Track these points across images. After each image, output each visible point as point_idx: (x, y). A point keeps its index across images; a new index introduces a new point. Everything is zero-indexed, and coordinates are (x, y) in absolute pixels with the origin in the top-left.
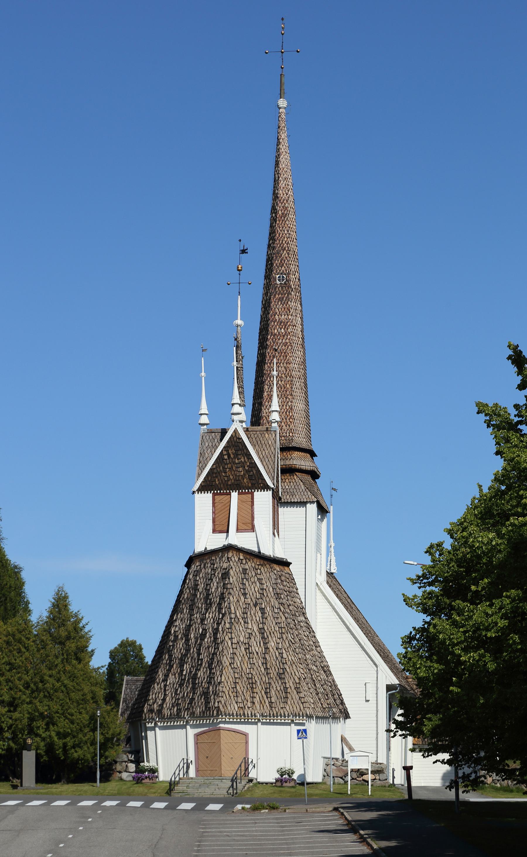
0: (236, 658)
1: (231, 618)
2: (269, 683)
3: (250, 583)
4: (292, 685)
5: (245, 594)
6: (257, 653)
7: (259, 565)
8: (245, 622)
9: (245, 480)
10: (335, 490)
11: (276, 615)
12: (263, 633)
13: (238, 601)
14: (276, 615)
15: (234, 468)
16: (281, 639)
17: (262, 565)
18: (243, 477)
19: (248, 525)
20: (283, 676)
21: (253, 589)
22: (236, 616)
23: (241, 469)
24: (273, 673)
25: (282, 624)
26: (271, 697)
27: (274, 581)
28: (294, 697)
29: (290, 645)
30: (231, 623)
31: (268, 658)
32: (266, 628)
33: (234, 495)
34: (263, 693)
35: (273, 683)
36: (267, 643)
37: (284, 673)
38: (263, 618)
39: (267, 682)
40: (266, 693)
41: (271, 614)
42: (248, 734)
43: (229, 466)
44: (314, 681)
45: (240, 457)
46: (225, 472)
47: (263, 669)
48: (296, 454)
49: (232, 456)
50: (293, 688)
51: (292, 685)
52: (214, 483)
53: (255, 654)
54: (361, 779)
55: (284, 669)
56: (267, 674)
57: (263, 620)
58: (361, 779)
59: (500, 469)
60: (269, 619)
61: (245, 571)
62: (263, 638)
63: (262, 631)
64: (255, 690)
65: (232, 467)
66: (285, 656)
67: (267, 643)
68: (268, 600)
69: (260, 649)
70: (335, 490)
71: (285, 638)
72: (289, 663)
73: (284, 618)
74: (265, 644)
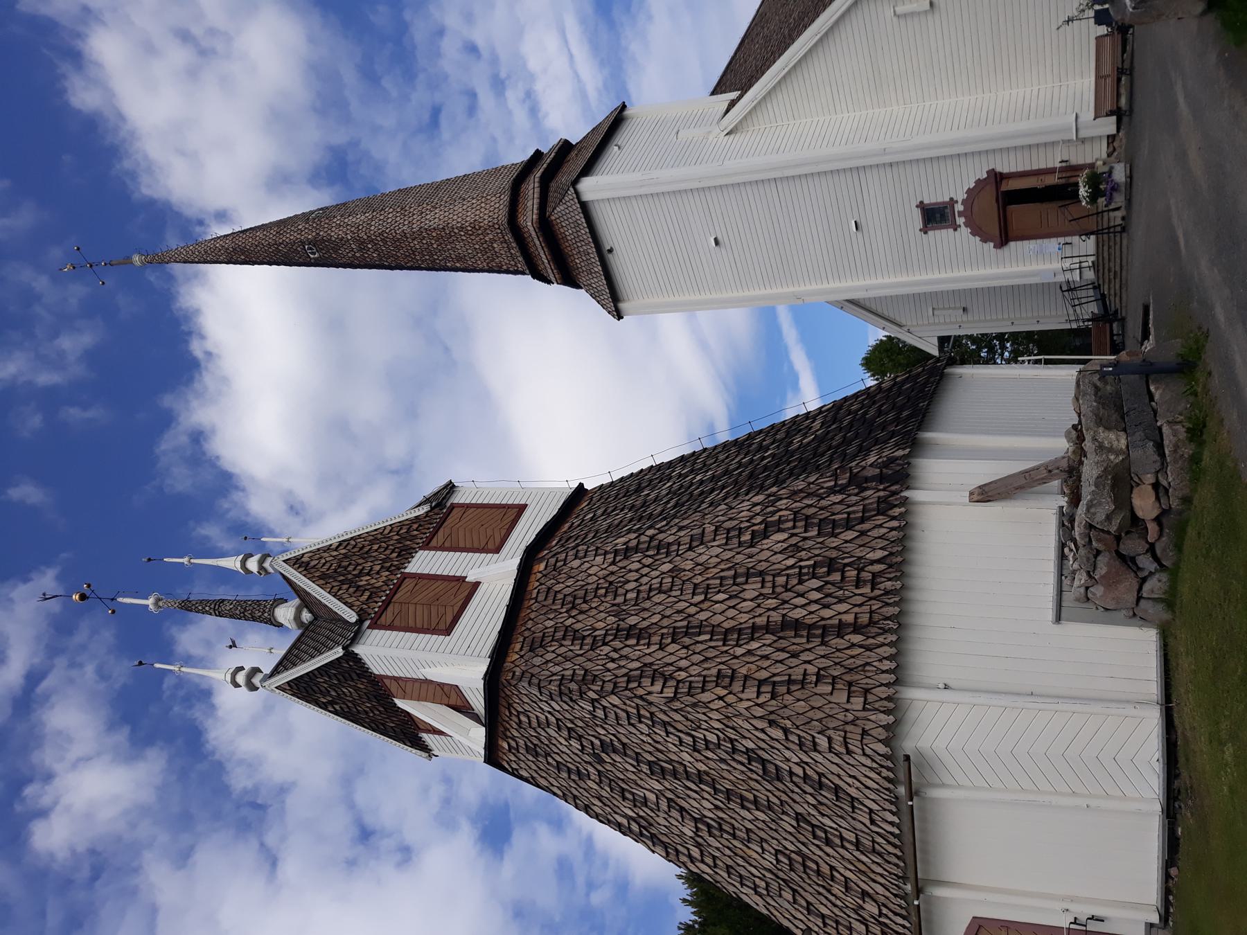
24: (763, 791)
26: (842, 838)
37: (763, 762)
54: (1152, 528)
58: (1152, 528)
61: (533, 750)
63: (657, 770)
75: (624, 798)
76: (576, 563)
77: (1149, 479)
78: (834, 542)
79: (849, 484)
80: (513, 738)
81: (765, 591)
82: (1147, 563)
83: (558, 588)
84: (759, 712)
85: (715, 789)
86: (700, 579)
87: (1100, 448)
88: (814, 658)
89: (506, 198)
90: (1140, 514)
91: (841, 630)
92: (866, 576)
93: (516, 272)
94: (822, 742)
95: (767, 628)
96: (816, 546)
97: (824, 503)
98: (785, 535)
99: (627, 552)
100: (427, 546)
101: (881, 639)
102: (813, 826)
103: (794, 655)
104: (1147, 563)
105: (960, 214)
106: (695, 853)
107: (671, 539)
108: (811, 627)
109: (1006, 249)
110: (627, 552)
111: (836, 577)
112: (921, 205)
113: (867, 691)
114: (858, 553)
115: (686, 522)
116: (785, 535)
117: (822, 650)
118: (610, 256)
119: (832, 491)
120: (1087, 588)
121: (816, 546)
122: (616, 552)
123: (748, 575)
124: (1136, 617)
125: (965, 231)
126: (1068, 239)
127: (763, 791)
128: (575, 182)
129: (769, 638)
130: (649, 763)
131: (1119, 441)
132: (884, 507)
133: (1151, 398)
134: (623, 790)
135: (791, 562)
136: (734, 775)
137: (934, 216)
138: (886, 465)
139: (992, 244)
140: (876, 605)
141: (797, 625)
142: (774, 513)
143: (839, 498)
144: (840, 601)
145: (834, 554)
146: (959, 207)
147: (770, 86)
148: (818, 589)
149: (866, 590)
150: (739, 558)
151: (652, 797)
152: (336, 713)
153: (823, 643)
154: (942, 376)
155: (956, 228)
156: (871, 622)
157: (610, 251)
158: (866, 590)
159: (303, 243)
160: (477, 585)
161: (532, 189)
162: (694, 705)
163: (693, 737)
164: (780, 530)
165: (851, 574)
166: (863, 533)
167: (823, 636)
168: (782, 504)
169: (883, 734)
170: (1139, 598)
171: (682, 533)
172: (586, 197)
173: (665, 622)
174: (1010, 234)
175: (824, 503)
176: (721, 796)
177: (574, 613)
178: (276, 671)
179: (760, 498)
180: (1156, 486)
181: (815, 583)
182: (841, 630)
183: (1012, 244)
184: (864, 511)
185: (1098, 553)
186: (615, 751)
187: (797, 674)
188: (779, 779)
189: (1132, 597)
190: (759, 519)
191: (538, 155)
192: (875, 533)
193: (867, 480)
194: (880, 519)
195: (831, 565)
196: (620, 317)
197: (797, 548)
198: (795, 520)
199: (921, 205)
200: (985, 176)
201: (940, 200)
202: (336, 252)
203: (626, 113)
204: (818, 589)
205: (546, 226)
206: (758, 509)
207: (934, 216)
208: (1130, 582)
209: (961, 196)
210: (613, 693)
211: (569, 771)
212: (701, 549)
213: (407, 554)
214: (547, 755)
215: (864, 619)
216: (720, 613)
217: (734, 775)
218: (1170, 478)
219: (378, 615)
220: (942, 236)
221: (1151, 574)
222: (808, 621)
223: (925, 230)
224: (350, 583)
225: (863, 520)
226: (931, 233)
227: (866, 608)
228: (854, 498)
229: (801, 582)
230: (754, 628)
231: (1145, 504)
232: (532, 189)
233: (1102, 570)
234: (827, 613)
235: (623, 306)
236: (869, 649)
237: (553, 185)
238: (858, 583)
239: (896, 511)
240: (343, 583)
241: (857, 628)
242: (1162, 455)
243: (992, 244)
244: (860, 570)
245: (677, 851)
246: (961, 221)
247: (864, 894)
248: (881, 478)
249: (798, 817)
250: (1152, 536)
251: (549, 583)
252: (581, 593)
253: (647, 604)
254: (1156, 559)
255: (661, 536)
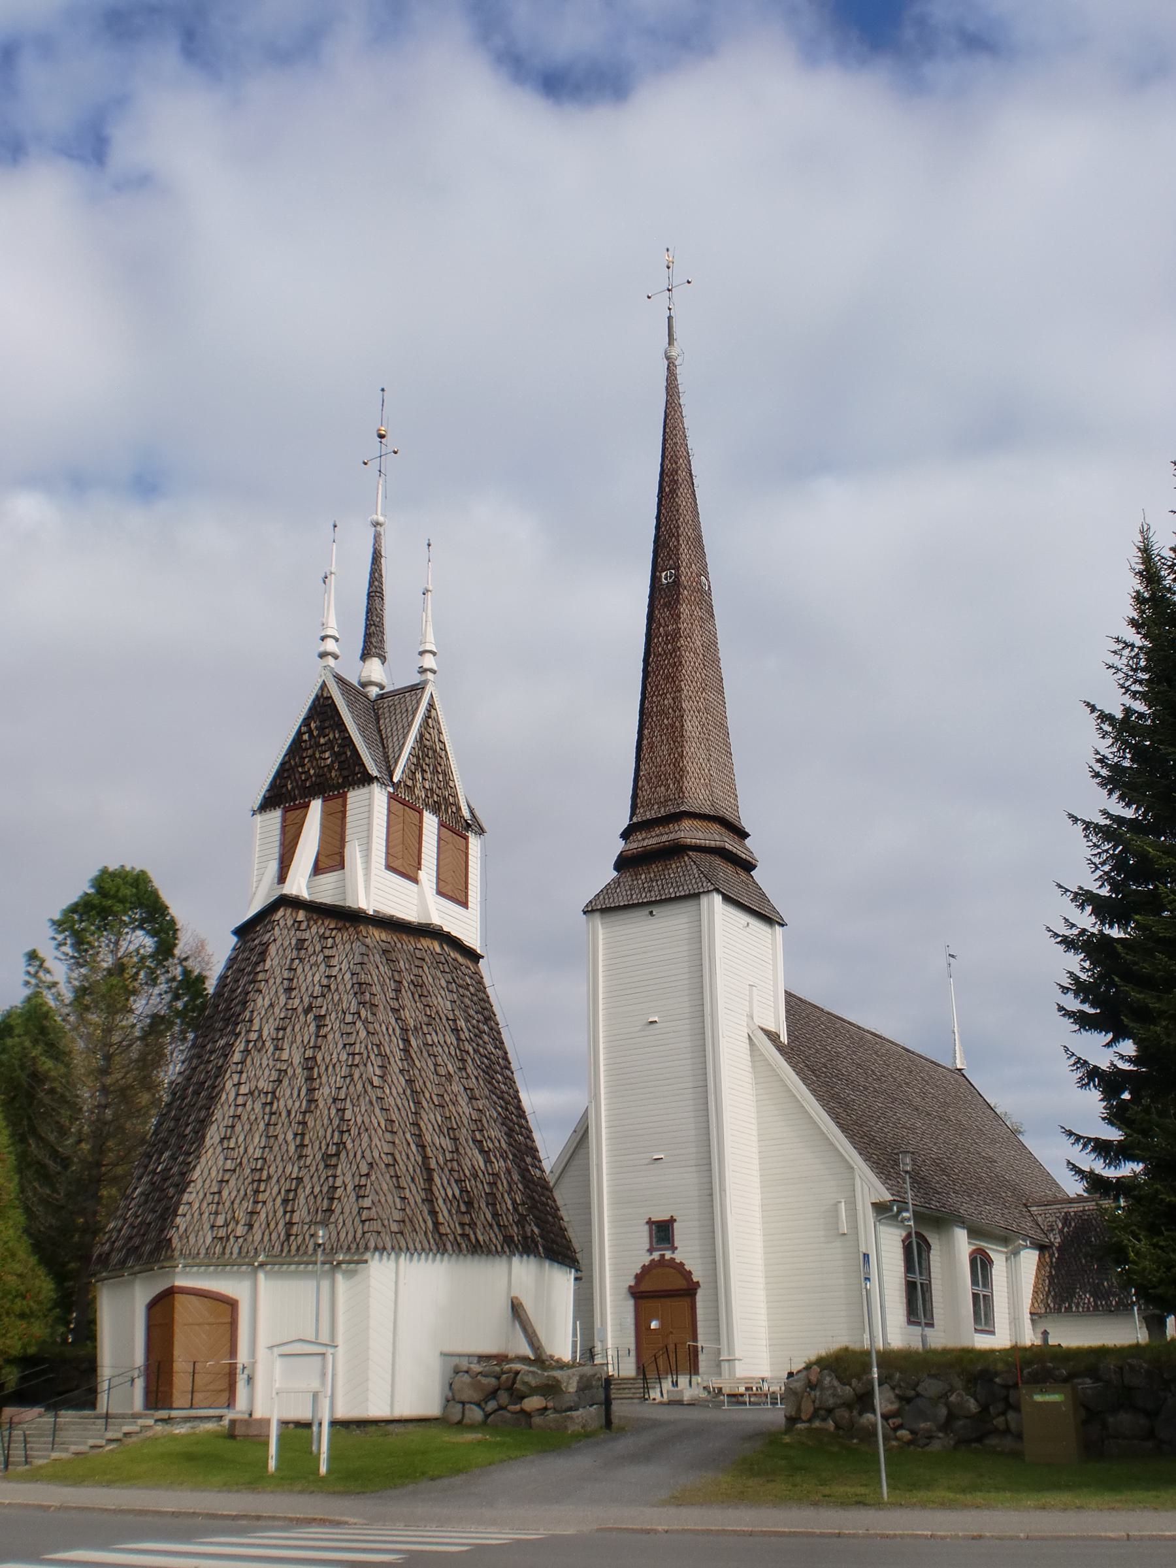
0: (238, 1128)
1: (248, 1042)
2: (297, 1178)
3: (307, 968)
4: (348, 1179)
5: (289, 990)
6: (289, 1112)
7: (332, 929)
8: (277, 1048)
9: (333, 774)
10: (953, 956)
11: (348, 1029)
12: (312, 1069)
13: (272, 1005)
14: (348, 1029)
15: (317, 756)
16: (348, 1080)
17: (339, 930)
18: (330, 767)
19: (331, 859)
20: (333, 1161)
21: (311, 978)
22: (260, 1036)
23: (327, 755)
24: (313, 1153)
25: (357, 1046)
26: (293, 1212)
27: (358, 959)
28: (347, 1210)
29: (366, 1091)
30: (247, 1051)
31: (311, 1124)
32: (319, 1058)
33: (316, 806)
34: (279, 1200)
35: (306, 1180)
36: (315, 1089)
37: (337, 1154)
38: (317, 1036)
39: (294, 1176)
40: (285, 1201)
41: (336, 1027)
42: (237, 1301)
43: (310, 752)
44: (430, 1171)
45: (327, 731)
46: (303, 766)
47: (292, 1148)
48: (686, 823)
49: (315, 733)
50: (350, 1187)
51: (348, 1179)
52: (284, 790)
53: (284, 1114)
54: (518, 1407)
55: (341, 1145)
56: (300, 1157)
57: (316, 1040)
58: (518, 1407)
59: (1089, 853)
60: (330, 1037)
61: (300, 944)
62: (310, 1079)
63: (309, 1064)
64: (261, 1197)
65: (314, 754)
66: (348, 1115)
67: (315, 1089)
68: (336, 998)
69: (297, 1104)
70: (953, 956)
71: (356, 1077)
72: (354, 1131)
73: (363, 1034)
74: (311, 1090)
75: (278, 1029)
76: (444, 984)
77: (550, 1404)
78: (483, 1205)
79: (519, 1214)
80: (309, 927)
81: (447, 1154)
82: (491, 1405)
83: (426, 968)
84: (376, 1154)
85: (305, 1112)
86: (447, 1099)
87: (569, 1378)
88: (415, 1194)
89: (707, 810)
90: (526, 1400)
91: (433, 1213)
92: (468, 1230)
93: (634, 807)
94: (367, 1203)
95: (425, 1158)
96: (479, 1189)
97: (506, 1195)
98: (483, 1168)
99: (456, 1031)
100: (442, 824)
101: (432, 1241)
102: (296, 1190)
103: (413, 1179)
104: (491, 1405)
105: (663, 1255)
106: (244, 1089)
107: (469, 1071)
108: (431, 1190)
109: (629, 1296)
110: (456, 1031)
111: (463, 1209)
112: (672, 1220)
113: (402, 1233)
114: (479, 1223)
115: (481, 1082)
116: (483, 1168)
117: (419, 1200)
118: (647, 912)
119: (514, 1201)
120: (467, 1372)
121: (479, 1189)
122: (454, 1020)
123: (455, 1139)
124: (448, 1401)
125: (646, 1259)
126: (633, 1353)
127: (313, 1153)
128: (718, 890)
129: (419, 1159)
130: (314, 1058)
131: (572, 1388)
132: (508, 1240)
133: (591, 1406)
134: (284, 1029)
135: (468, 1174)
136: (320, 1126)
137: (662, 1232)
138: (533, 1241)
139: (632, 1284)
140: (451, 1237)
141: (430, 1180)
142: (495, 1156)
143: (511, 1208)
144: (450, 1212)
145: (476, 1206)
146: (668, 1255)
147: (788, 1083)
148: (454, 1195)
149: (459, 1231)
150: (464, 1131)
151: (285, 1056)
152: (299, 733)
153: (423, 1201)
154: (571, 1267)
155: (651, 1251)
156: (441, 1235)
157: (651, 913)
158: (459, 1231)
159: (677, 568)
160: (415, 881)
161: (712, 836)
162: (371, 1102)
163: (345, 1099)
164: (485, 1163)
165: (467, 1219)
166: (491, 1226)
167: (427, 1200)
168: (502, 1163)
169: (380, 1245)
170: (463, 1403)
171: (474, 1080)
172: (704, 900)
173: (417, 1072)
174: (640, 1301)
175: (506, 1195)
176: (300, 1117)
177: (412, 987)
178: (340, 680)
179: (504, 1145)
180: (546, 1409)
181: (457, 1193)
182: (433, 1213)
183: (631, 1302)
184: (504, 1226)
185: (498, 1378)
186: (319, 1027)
187: (403, 1184)
188: (327, 1166)
189: (465, 1398)
190: (491, 1145)
191: (743, 835)
192: (492, 1235)
193: (523, 1227)
194: (501, 1238)
195: (469, 1204)
196: (585, 913)
197: (476, 1176)
198: (493, 1174)
199: (672, 1220)
200: (695, 1280)
201: (676, 1237)
202: (665, 605)
203: (777, 927)
204: (454, 1195)
205: (677, 850)
206: (497, 1144)
207: (662, 1232)
208: (476, 1397)
209: (678, 1257)
210: (368, 1032)
211: (291, 980)
212: (466, 1098)
213: (436, 810)
214: (301, 960)
215: (443, 1230)
216: (430, 1118)
217: (320, 1126)
218: (551, 1415)
219: (405, 805)
220: (643, 1237)
221: (483, 1410)
222: (434, 1188)
223: (650, 1222)
224: (417, 765)
225: (499, 1225)
226: (646, 1227)
227: (449, 1231)
228: (511, 1218)
229: (456, 1181)
230: (424, 1147)
231: (533, 1403)
232: (712, 836)
233: (484, 1380)
234: (440, 1201)
235: (597, 918)
236: (426, 1233)
237: (717, 861)
238: (462, 1225)
239: (507, 1249)
240: (418, 757)
241: (436, 1224)
242: (566, 1411)
243: (632, 1284)
244: (469, 1225)
245: (241, 1072)
246: (656, 1255)
247: (250, 1226)
248: (525, 1237)
249: (300, 1180)
250: (511, 1408)
251: (427, 959)
252: (426, 993)
253: (425, 1054)
254: (495, 1411)
255: (469, 1061)
